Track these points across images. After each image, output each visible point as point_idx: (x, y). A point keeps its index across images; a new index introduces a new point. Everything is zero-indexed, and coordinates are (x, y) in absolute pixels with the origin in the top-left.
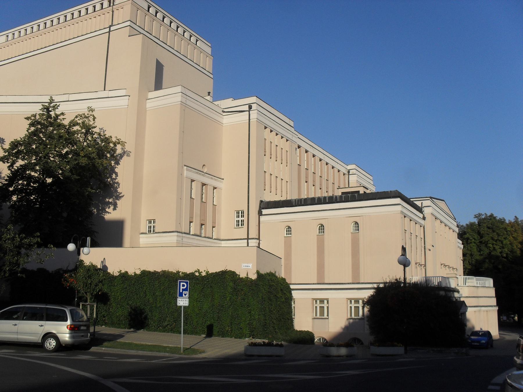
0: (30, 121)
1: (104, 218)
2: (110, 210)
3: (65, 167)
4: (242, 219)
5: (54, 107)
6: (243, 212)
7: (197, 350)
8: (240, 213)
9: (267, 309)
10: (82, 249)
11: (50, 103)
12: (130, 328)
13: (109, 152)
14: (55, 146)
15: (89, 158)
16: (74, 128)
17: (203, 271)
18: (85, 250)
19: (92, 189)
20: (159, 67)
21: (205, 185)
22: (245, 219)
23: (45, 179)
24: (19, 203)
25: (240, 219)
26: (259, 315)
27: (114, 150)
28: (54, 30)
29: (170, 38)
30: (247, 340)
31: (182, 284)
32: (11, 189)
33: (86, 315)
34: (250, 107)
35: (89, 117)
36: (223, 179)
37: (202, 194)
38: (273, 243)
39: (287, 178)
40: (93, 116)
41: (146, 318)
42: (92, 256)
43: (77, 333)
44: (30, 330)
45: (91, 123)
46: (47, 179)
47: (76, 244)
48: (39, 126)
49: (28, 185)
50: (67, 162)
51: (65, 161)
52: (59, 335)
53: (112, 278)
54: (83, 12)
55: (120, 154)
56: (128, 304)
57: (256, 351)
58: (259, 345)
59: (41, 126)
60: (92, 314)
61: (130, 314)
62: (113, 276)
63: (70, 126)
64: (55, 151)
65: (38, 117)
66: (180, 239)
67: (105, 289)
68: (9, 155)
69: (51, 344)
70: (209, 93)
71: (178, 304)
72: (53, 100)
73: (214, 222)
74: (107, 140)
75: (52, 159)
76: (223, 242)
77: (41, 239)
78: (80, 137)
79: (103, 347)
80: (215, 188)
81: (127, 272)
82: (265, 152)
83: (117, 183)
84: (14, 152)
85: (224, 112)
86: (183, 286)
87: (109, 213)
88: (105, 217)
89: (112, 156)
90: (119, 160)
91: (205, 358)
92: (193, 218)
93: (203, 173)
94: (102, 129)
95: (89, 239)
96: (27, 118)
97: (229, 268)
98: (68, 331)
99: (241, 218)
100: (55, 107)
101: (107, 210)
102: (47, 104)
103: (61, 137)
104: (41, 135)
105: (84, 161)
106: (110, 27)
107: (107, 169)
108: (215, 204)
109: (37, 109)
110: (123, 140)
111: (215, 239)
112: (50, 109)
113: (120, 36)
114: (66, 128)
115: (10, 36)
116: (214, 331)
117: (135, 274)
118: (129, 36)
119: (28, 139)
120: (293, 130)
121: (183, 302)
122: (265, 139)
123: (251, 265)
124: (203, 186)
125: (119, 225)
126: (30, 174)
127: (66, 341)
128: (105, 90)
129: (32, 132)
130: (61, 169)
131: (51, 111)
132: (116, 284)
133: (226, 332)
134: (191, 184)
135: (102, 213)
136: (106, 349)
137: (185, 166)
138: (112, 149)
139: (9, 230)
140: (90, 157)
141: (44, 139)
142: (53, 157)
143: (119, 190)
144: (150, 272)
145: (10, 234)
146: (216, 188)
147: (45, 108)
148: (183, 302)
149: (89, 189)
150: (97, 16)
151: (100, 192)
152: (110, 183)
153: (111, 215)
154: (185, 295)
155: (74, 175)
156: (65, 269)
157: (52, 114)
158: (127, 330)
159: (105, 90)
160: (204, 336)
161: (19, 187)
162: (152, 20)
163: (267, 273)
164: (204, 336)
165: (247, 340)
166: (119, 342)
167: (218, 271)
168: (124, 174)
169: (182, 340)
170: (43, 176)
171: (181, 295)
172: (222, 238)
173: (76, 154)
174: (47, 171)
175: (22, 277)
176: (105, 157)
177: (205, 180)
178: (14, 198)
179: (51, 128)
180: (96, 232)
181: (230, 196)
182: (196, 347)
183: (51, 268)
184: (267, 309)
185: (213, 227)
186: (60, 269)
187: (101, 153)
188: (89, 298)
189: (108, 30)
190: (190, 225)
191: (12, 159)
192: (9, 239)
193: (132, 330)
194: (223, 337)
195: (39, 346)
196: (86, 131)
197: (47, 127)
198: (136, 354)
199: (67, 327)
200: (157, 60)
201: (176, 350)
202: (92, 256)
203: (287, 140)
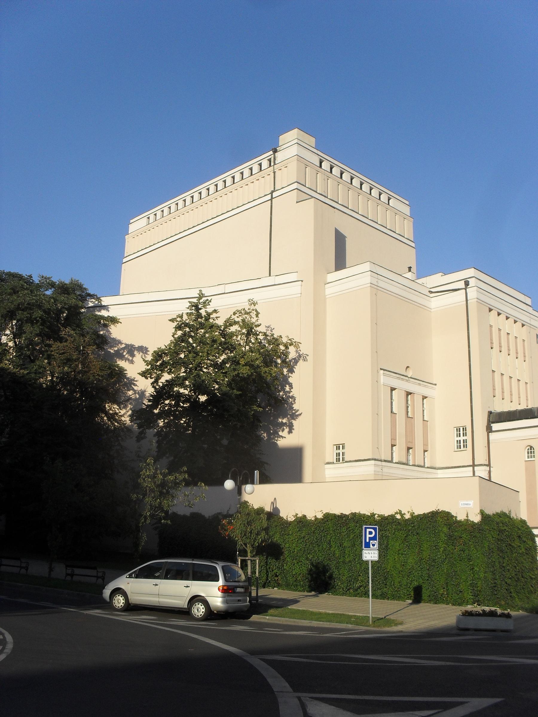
0: (176, 323)
1: (276, 444)
2: (284, 433)
3: (223, 380)
4: (465, 438)
5: (204, 303)
6: (465, 429)
7: (393, 620)
8: (460, 431)
9: (497, 564)
10: (243, 487)
11: (200, 298)
12: (310, 591)
13: (280, 357)
14: (208, 354)
15: (251, 366)
16: (231, 328)
17: (406, 513)
18: (248, 488)
19: (259, 406)
20: (340, 240)
21: (411, 393)
22: (469, 438)
23: (197, 397)
24: (166, 429)
25: (462, 438)
26: (485, 572)
27: (286, 354)
28: (260, 178)
29: (351, 199)
30: (458, 610)
31: (368, 530)
32: (156, 411)
33: (246, 574)
34: (467, 284)
35: (250, 312)
36: (436, 385)
37: (407, 407)
38: (509, 469)
39: (525, 378)
40: (256, 311)
41: (331, 577)
42: (259, 495)
43: (231, 596)
44: (173, 592)
45: (253, 320)
46: (199, 397)
47: (234, 479)
48: (187, 329)
49: (177, 405)
50: (224, 373)
51: (222, 373)
52: (209, 599)
53: (285, 524)
54: (238, 177)
55: (294, 359)
56: (307, 559)
57: (472, 623)
58: (478, 615)
59: (190, 328)
60: (254, 572)
61: (310, 572)
62: (287, 521)
63: (226, 327)
64: (208, 359)
65: (185, 317)
66: (379, 469)
67: (277, 539)
68: (152, 369)
69: (199, 610)
70: (410, 268)
71: (364, 559)
72: (202, 294)
73: (425, 444)
74: (276, 342)
75: (205, 370)
76: (439, 471)
77: (189, 475)
78: (240, 339)
79: (267, 616)
80: (424, 398)
81: (305, 516)
82: (492, 343)
83: (292, 397)
84: (158, 364)
85: (431, 292)
86: (370, 533)
87: (282, 436)
88: (278, 442)
89: (284, 361)
90: (293, 367)
91: (401, 632)
92: (396, 440)
93: (407, 378)
94: (268, 327)
95: (257, 473)
96: (172, 320)
97: (441, 508)
98: (220, 594)
99: (463, 436)
100: (206, 304)
101: (280, 433)
102: (195, 300)
103: (214, 341)
104: (190, 340)
105: (245, 371)
106: (272, 193)
107: (277, 379)
108: (425, 419)
109: (182, 308)
110: (296, 339)
111: (428, 468)
112: (200, 307)
113: (286, 203)
114: (220, 330)
115: (152, 217)
116: (423, 595)
117: (316, 519)
118: (297, 202)
119: (175, 346)
120: (530, 310)
121: (370, 555)
122: (491, 326)
123: (471, 502)
124: (407, 395)
125: (297, 453)
126: (178, 392)
127: (217, 607)
128: (270, 275)
129: (179, 338)
130: (217, 383)
131: (201, 309)
132: (290, 533)
133: (439, 596)
134: (391, 393)
135: (274, 438)
136: (271, 618)
137: (381, 369)
138: (282, 353)
139: (148, 465)
140: (253, 365)
141: (194, 345)
142: (206, 368)
143: (295, 407)
144: (335, 515)
145: (150, 470)
146: (426, 397)
147: (193, 306)
148: (370, 555)
149: (255, 408)
150: (260, 178)
151: (270, 410)
152: (282, 398)
153: (286, 440)
154: (373, 545)
155: (233, 389)
156: (225, 513)
157: (203, 312)
158: (306, 593)
159: (270, 275)
160: (410, 601)
161: (166, 408)
162: (326, 178)
163: (497, 513)
164: (410, 601)
165: (458, 610)
166: (290, 609)
167: (426, 511)
168: (300, 385)
169: (370, 608)
170: (195, 394)
171: (367, 545)
172: (438, 466)
173: (235, 362)
174: (199, 387)
175: (167, 523)
176: (273, 364)
177: (411, 387)
178: (161, 423)
179: (203, 331)
180: (267, 464)
181: (446, 407)
182: (392, 617)
183: (208, 512)
184: (497, 564)
185: (425, 451)
186: (220, 513)
187: (268, 359)
188: (249, 551)
189: (269, 197)
190: (392, 450)
191: (156, 373)
192: (148, 476)
193: (313, 593)
194: (436, 603)
195: (184, 613)
196: (248, 331)
197: (197, 329)
198: (309, 625)
199: (219, 589)
200: (337, 231)
201: (363, 621)
202: (259, 495)
203: (523, 325)
